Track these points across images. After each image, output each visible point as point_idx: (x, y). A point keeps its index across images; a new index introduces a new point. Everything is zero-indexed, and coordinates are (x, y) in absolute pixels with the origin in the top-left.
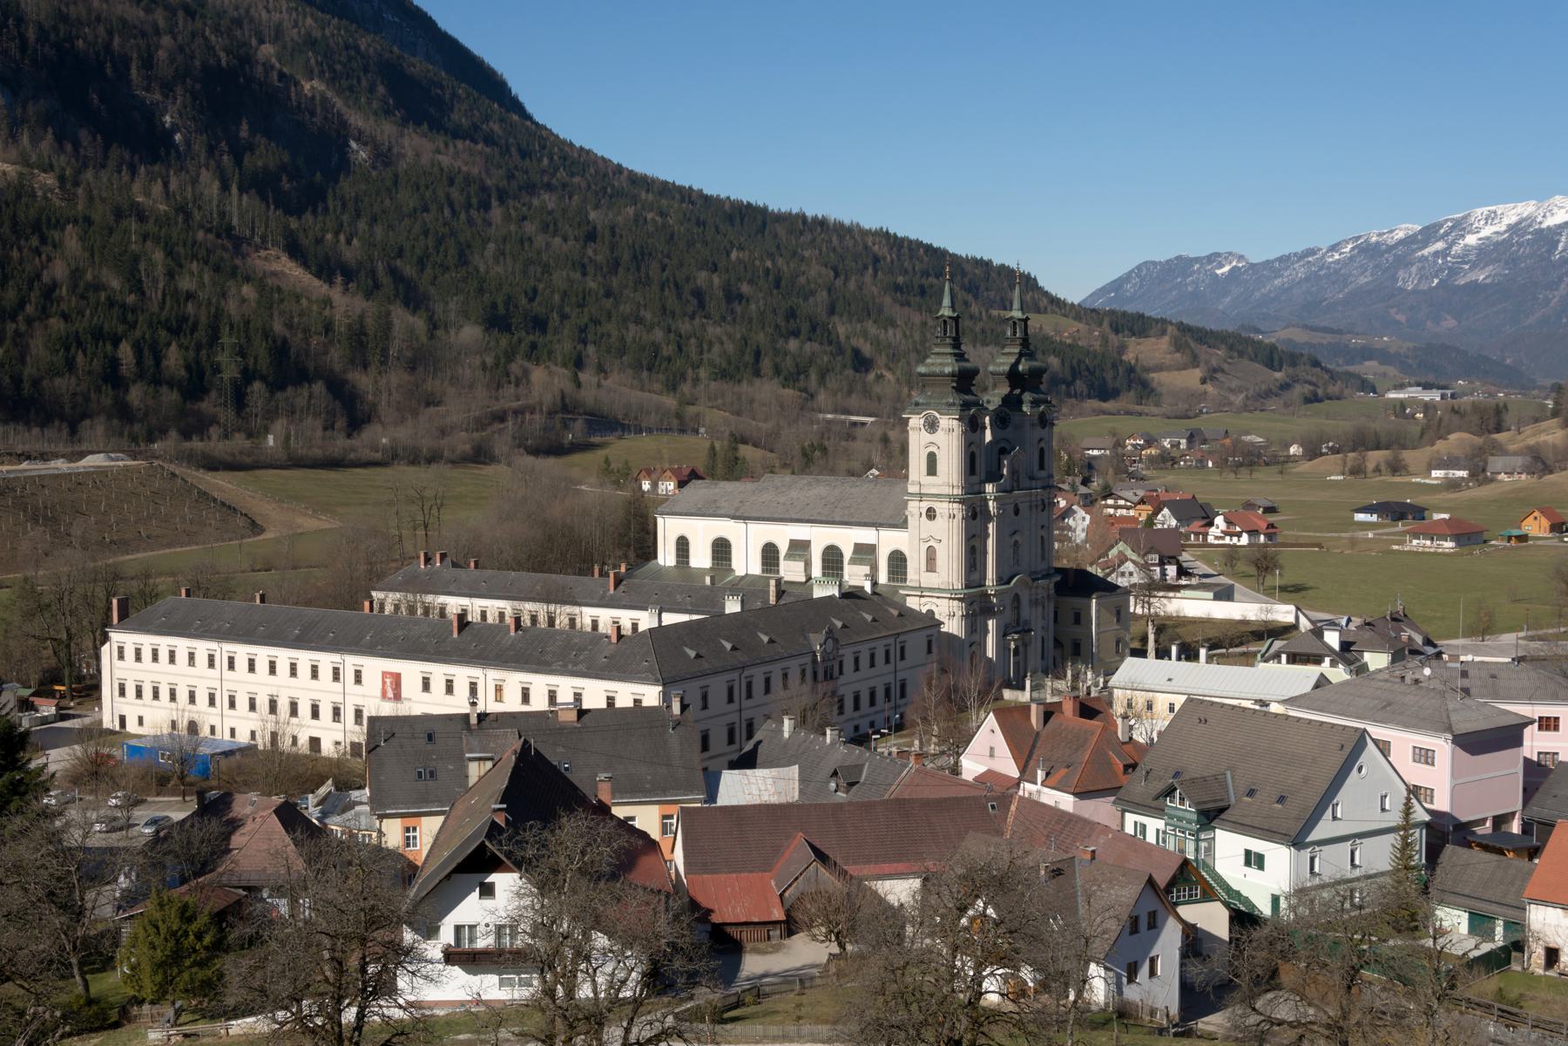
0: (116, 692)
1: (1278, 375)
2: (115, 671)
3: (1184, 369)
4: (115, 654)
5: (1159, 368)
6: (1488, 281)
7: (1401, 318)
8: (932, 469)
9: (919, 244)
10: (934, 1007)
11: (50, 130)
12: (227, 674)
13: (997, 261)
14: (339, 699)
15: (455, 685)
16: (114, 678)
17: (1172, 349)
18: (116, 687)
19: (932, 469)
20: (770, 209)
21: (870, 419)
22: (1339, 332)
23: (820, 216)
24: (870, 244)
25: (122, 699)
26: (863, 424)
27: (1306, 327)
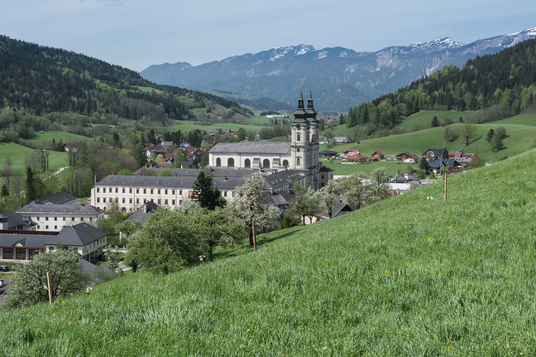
0: (96, 201)
1: (229, 110)
2: (96, 195)
3: (201, 108)
4: (96, 191)
5: (192, 108)
6: (279, 75)
7: (249, 88)
8: (299, 139)
9: (101, 61)
10: (526, 217)
11: (326, 56)
12: (136, 194)
13: (124, 67)
14: (174, 199)
15: (126, 200)
16: (96, 198)
17: (195, 101)
18: (96, 200)
19: (299, 139)
20: (39, 45)
21: (113, 126)
22: (230, 93)
23: (59, 49)
24: (80, 60)
25: (98, 203)
26: (112, 127)
27: (218, 91)
